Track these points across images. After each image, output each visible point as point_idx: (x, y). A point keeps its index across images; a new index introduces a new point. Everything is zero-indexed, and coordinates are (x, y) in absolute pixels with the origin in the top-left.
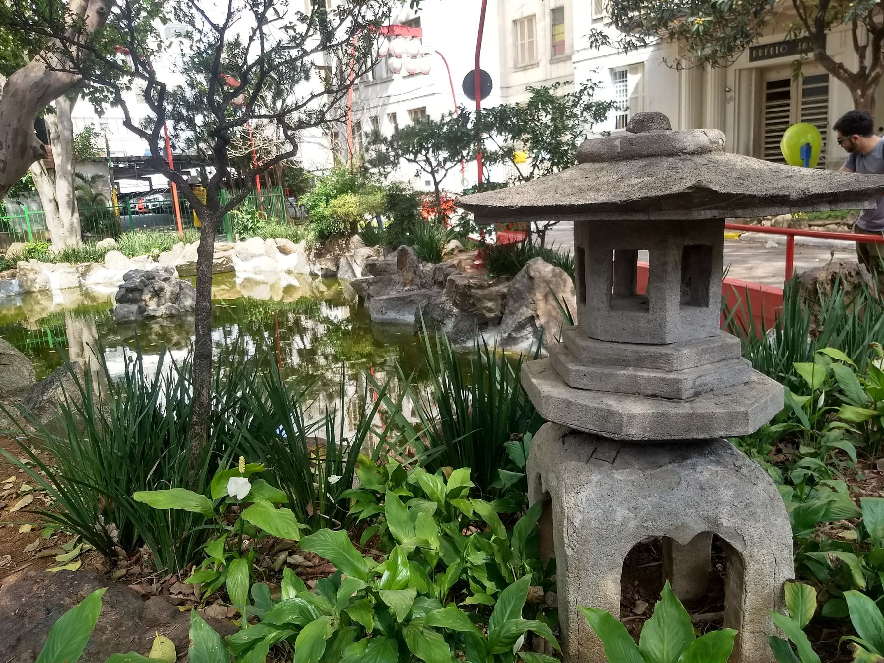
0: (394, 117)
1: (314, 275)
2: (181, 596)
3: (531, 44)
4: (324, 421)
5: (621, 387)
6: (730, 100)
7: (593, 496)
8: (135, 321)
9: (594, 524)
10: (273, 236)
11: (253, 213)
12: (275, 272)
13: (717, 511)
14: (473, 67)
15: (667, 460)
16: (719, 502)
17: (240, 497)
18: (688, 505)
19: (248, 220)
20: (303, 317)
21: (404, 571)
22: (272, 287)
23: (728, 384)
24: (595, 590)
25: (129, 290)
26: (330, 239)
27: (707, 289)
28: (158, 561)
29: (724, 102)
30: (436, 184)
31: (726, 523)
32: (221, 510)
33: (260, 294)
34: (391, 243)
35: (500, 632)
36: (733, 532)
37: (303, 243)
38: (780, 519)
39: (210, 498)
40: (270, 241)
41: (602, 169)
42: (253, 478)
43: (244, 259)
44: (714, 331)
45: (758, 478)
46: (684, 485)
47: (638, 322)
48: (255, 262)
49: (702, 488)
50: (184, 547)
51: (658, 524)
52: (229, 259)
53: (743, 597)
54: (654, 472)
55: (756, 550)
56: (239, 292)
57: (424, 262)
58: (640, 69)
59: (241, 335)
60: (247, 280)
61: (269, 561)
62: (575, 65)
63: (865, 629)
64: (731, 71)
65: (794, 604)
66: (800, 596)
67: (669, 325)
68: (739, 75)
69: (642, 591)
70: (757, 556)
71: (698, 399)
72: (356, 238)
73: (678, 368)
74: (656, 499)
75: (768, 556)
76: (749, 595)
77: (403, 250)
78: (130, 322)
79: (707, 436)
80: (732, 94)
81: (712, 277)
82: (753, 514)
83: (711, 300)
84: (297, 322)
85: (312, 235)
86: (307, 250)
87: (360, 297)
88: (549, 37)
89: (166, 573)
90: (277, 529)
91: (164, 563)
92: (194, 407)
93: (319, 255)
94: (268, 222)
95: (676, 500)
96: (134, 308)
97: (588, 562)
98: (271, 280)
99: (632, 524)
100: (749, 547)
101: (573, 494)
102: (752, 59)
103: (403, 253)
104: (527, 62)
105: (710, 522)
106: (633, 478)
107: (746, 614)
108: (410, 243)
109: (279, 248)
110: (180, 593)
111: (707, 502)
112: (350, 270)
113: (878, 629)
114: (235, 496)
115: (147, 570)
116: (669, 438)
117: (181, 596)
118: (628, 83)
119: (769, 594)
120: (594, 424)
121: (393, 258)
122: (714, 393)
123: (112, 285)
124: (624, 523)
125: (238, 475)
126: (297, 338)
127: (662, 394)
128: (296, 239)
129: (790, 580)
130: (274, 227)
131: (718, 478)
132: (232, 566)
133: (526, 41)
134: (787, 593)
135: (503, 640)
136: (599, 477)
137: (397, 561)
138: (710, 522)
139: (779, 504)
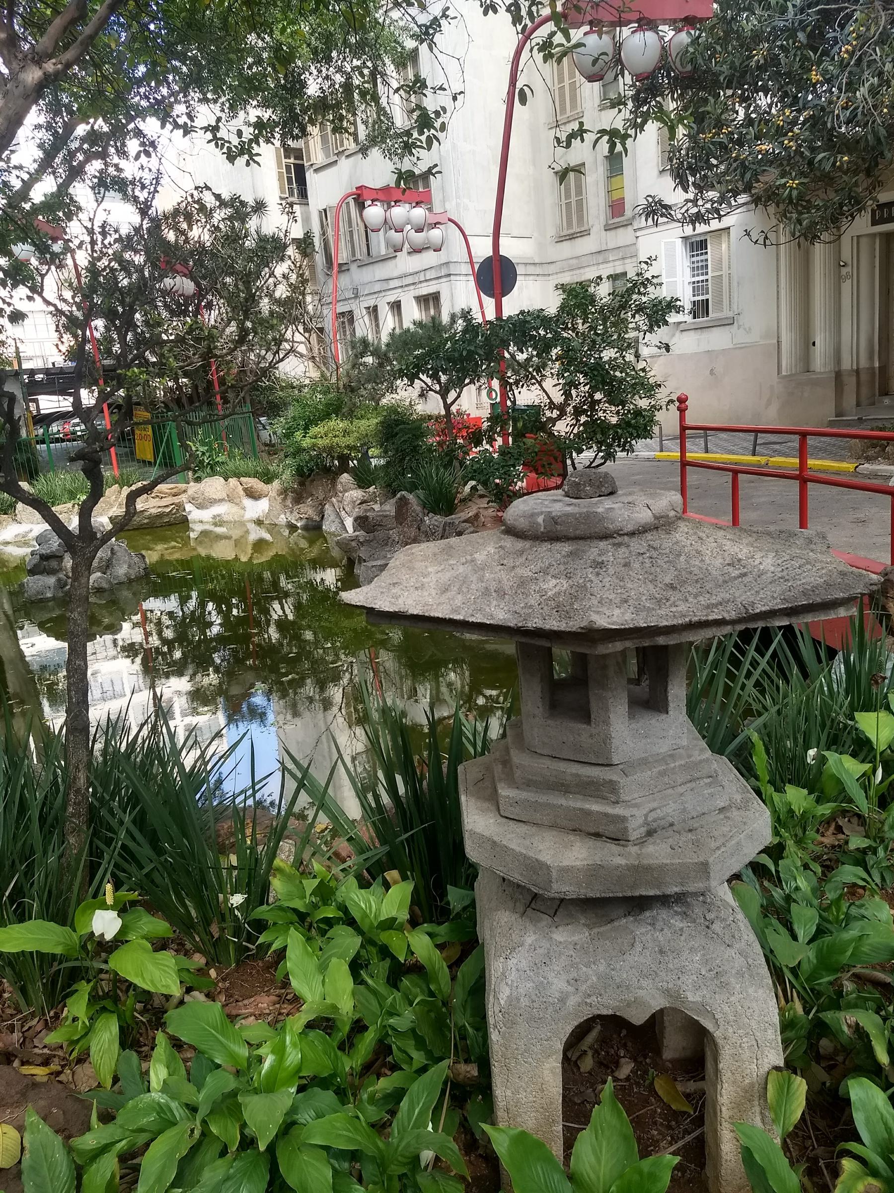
0: (396, 306)
1: (292, 528)
2: (46, 1051)
3: (580, 203)
4: (257, 788)
5: (558, 821)
6: (846, 277)
7: (524, 964)
8: (53, 598)
9: (524, 1002)
10: (238, 475)
11: (209, 444)
12: (242, 524)
13: (679, 983)
14: (490, 253)
15: (621, 912)
16: (682, 970)
17: (109, 937)
18: (643, 975)
19: (203, 454)
20: (282, 578)
21: (294, 1053)
22: (237, 543)
23: (695, 814)
24: (528, 1086)
25: (44, 558)
26: (313, 476)
27: (666, 691)
28: (22, 1002)
29: (839, 280)
30: (447, 407)
31: (692, 997)
32: (89, 947)
33: (223, 552)
34: (389, 485)
35: (398, 1146)
36: (701, 1008)
37: (276, 484)
38: (761, 991)
39: (75, 931)
40: (233, 481)
41: (521, 553)
42: (123, 910)
43: (200, 507)
44: (678, 741)
45: (733, 937)
46: (638, 947)
47: (579, 735)
48: (217, 510)
49: (661, 952)
50: (54, 983)
51: (605, 1000)
52: (180, 506)
53: (719, 1087)
54: (602, 929)
55: (731, 1030)
56: (195, 549)
57: (431, 515)
58: (724, 238)
59: (202, 605)
60: (204, 533)
61: (143, 1021)
62: (638, 234)
63: (871, 1132)
64: (846, 240)
65: (777, 1102)
66: (785, 1091)
67: (616, 742)
68: (858, 243)
69: (629, 1044)
70: (734, 1039)
71: (651, 840)
72: (345, 477)
73: (627, 798)
74: (602, 968)
75: (750, 1032)
76: (725, 1085)
77: (403, 498)
78: (48, 600)
79: (658, 893)
80: (849, 269)
81: (670, 677)
82: (724, 986)
83: (672, 705)
84: (275, 583)
85: (287, 475)
86: (281, 494)
87: (349, 559)
88: (602, 193)
89: (33, 1015)
90: (152, 982)
91: (29, 1004)
92: (68, 794)
93: (299, 499)
94: (231, 456)
95: (627, 968)
96: (51, 580)
97: (517, 1049)
98: (236, 533)
99: (572, 1001)
100: (721, 1027)
101: (502, 959)
102: (874, 223)
103: (403, 502)
104: (575, 229)
105: (671, 996)
106: (576, 938)
107: (724, 1109)
108: (412, 488)
109: (245, 490)
110: (45, 1047)
111: (669, 970)
112: (337, 520)
113: (888, 1129)
114: (102, 935)
115: (9, 1011)
116: (611, 895)
117: (46, 1051)
118: (709, 256)
119: (752, 1085)
120: (522, 874)
121: (390, 508)
122: (675, 828)
123: (26, 544)
124: (563, 1000)
125: (104, 906)
126: (276, 606)
127: (607, 834)
128: (267, 477)
129: (777, 1068)
130: (238, 463)
131: (683, 938)
132: (99, 1024)
133: (573, 199)
134: (769, 1086)
135: (400, 1158)
136: (533, 938)
137: (285, 1041)
138: (671, 996)
139: (760, 971)
